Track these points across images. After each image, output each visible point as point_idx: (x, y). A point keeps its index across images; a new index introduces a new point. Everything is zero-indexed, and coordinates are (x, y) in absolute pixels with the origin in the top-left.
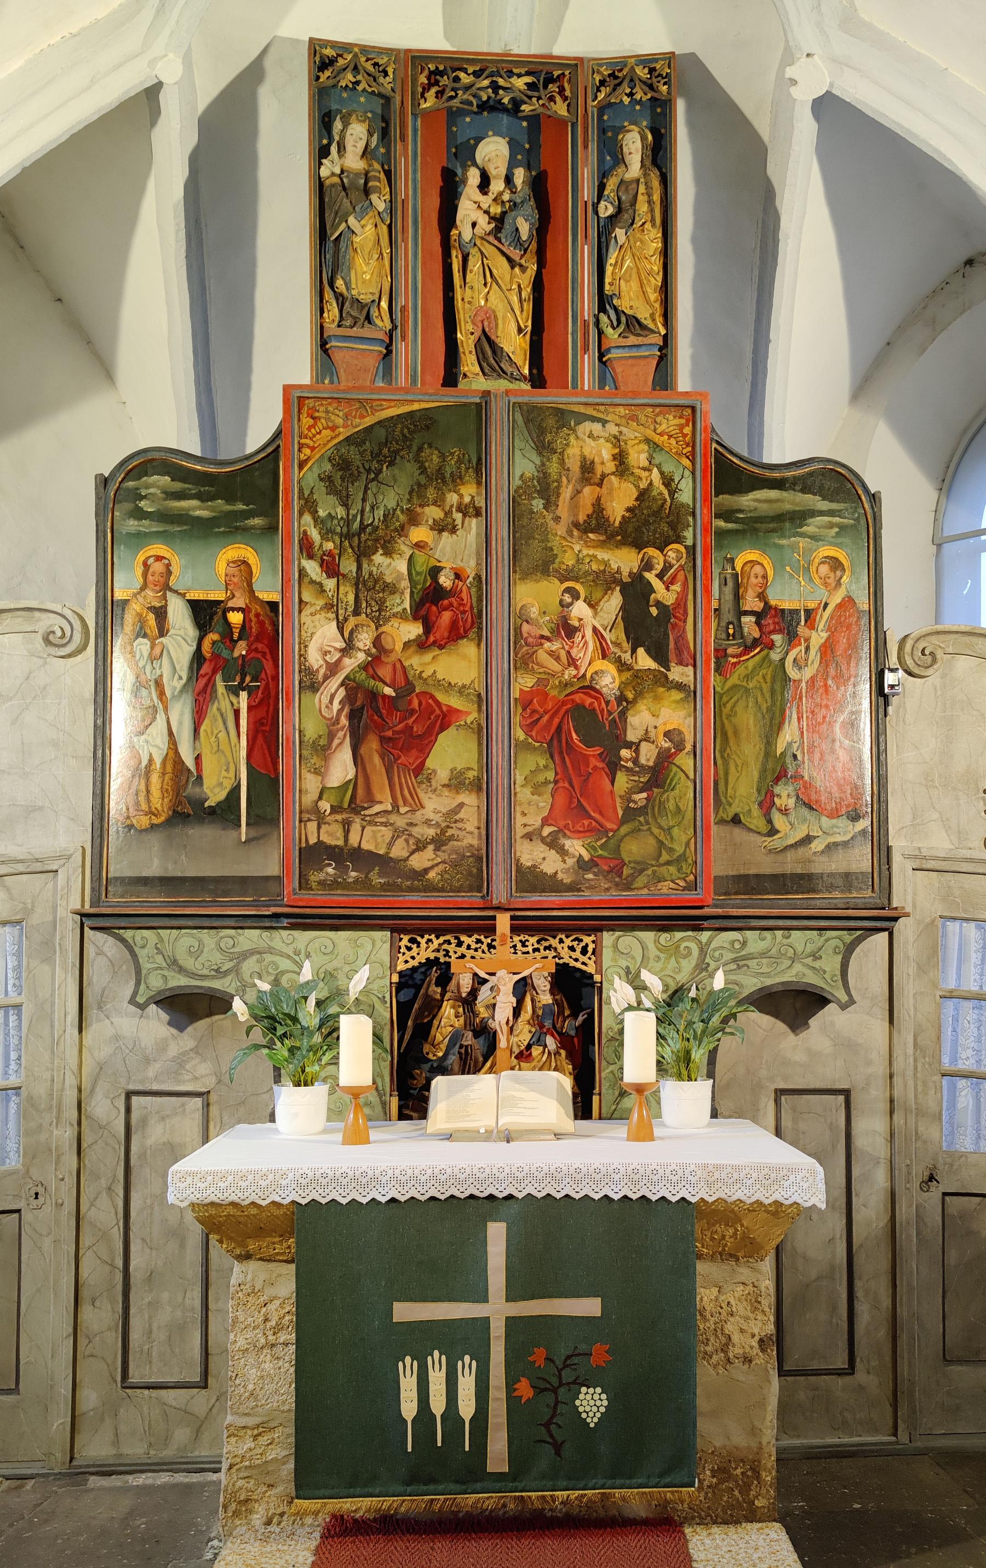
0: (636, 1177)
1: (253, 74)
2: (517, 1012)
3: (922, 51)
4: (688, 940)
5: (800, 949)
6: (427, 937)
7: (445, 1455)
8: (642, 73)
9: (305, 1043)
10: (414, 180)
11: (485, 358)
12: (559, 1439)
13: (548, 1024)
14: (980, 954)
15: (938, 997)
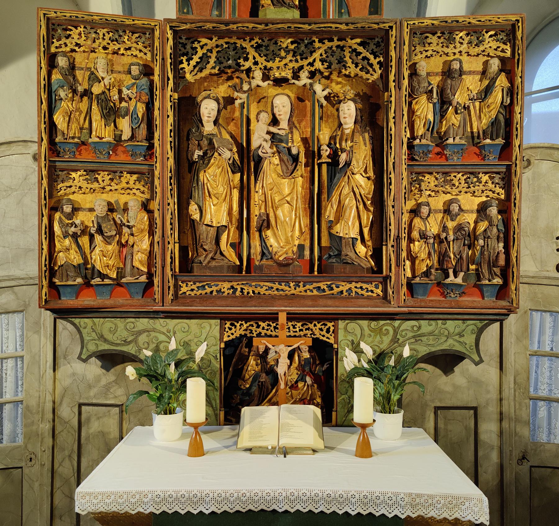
0: (366, 501)
4: (388, 326)
5: (451, 330)
6: (240, 322)
13: (307, 369)
14: (551, 330)
15: (528, 355)
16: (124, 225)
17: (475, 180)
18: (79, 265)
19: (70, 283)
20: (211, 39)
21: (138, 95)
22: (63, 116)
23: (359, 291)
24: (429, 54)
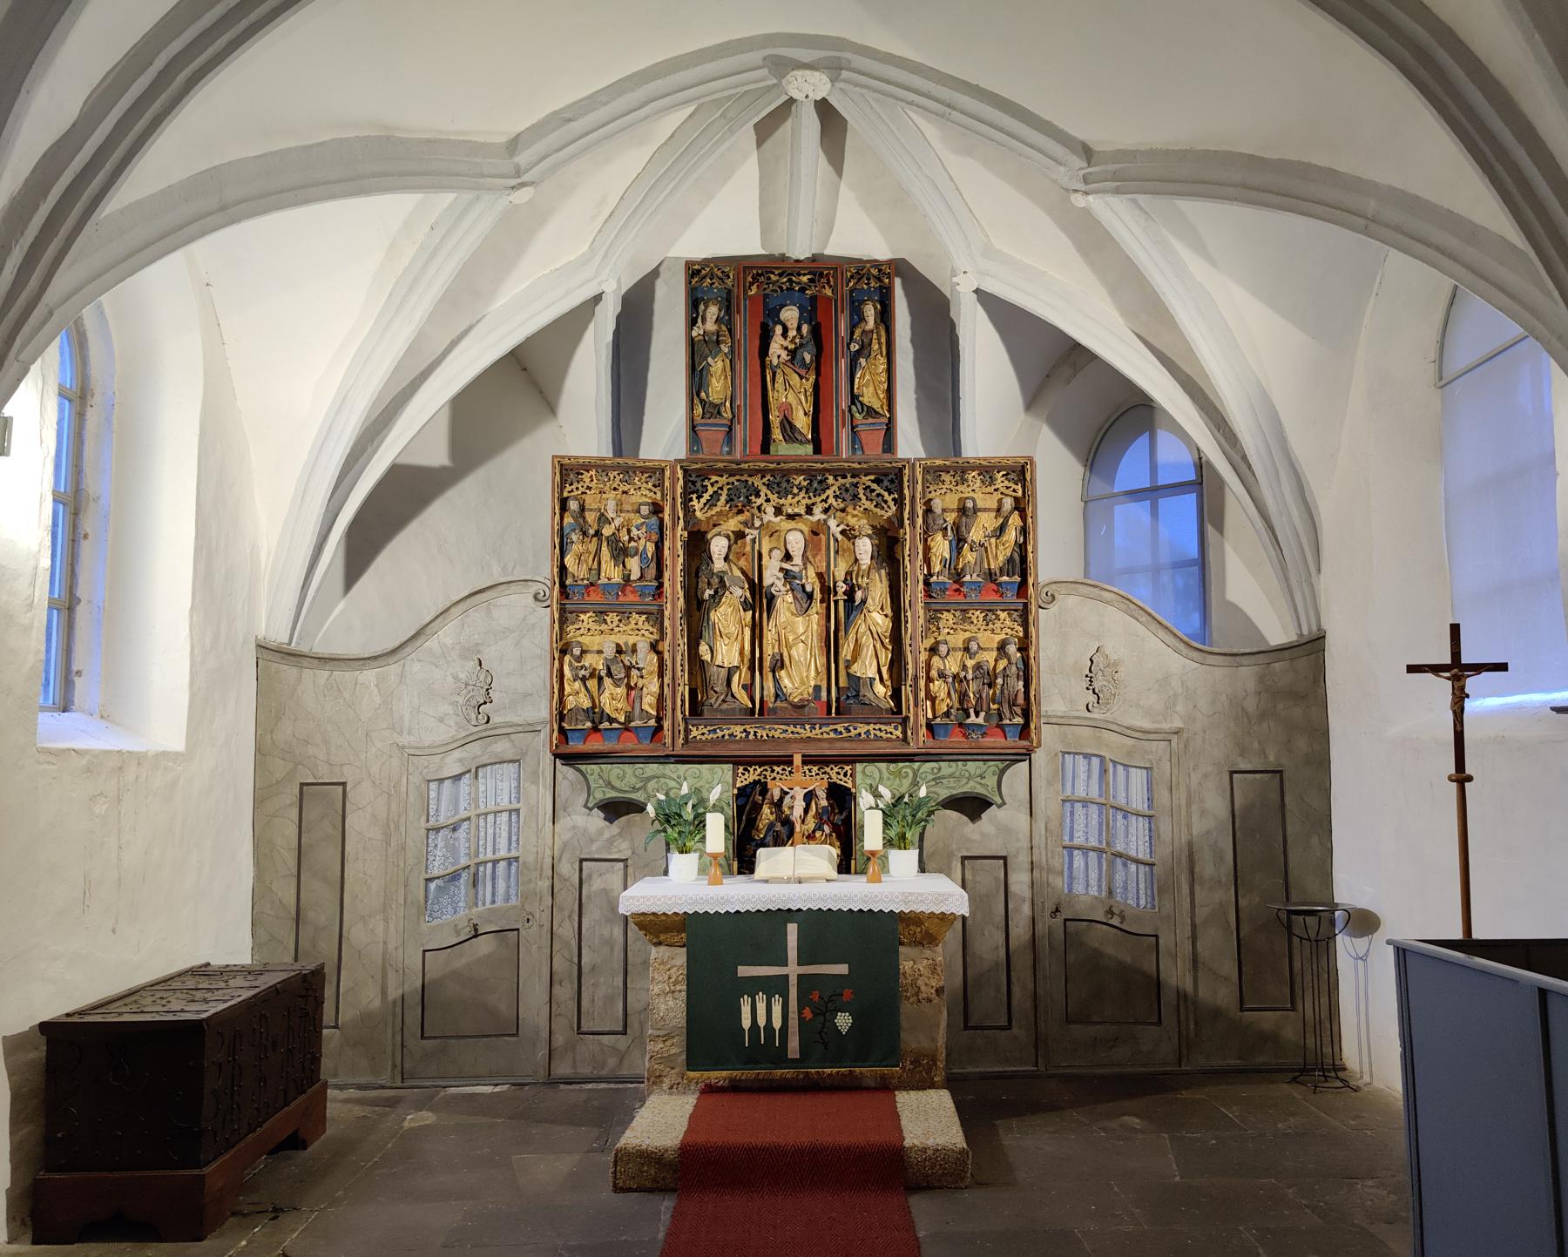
1: (655, 273)
2: (806, 811)
7: (766, 1049)
8: (874, 272)
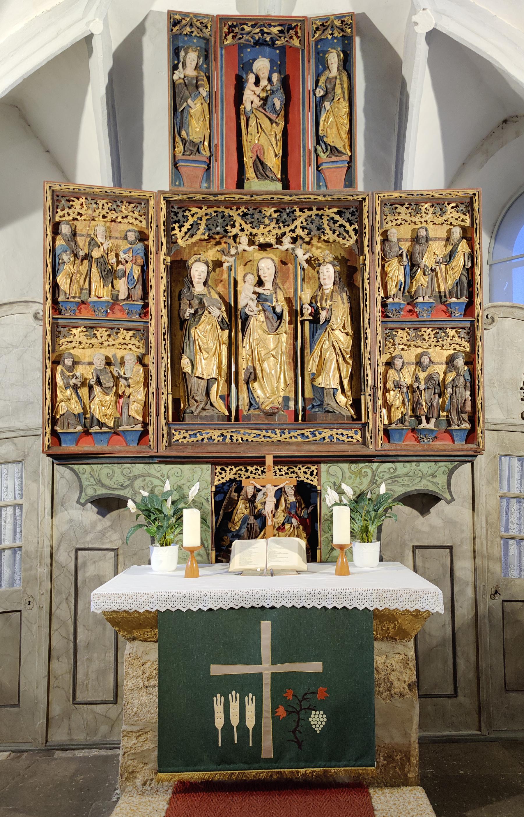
0: (340, 597)
1: (140, 30)
2: (277, 506)
3: (483, 7)
5: (425, 472)
6: (230, 467)
7: (239, 748)
8: (338, 23)
9: (165, 524)
10: (221, 80)
11: (258, 170)
12: (300, 740)
13: (293, 512)
14: (520, 474)
16: (121, 377)
17: (443, 334)
18: (79, 414)
19: (71, 430)
20: (201, 208)
21: (134, 258)
22: (66, 278)
23: (340, 437)
24: (398, 222)
